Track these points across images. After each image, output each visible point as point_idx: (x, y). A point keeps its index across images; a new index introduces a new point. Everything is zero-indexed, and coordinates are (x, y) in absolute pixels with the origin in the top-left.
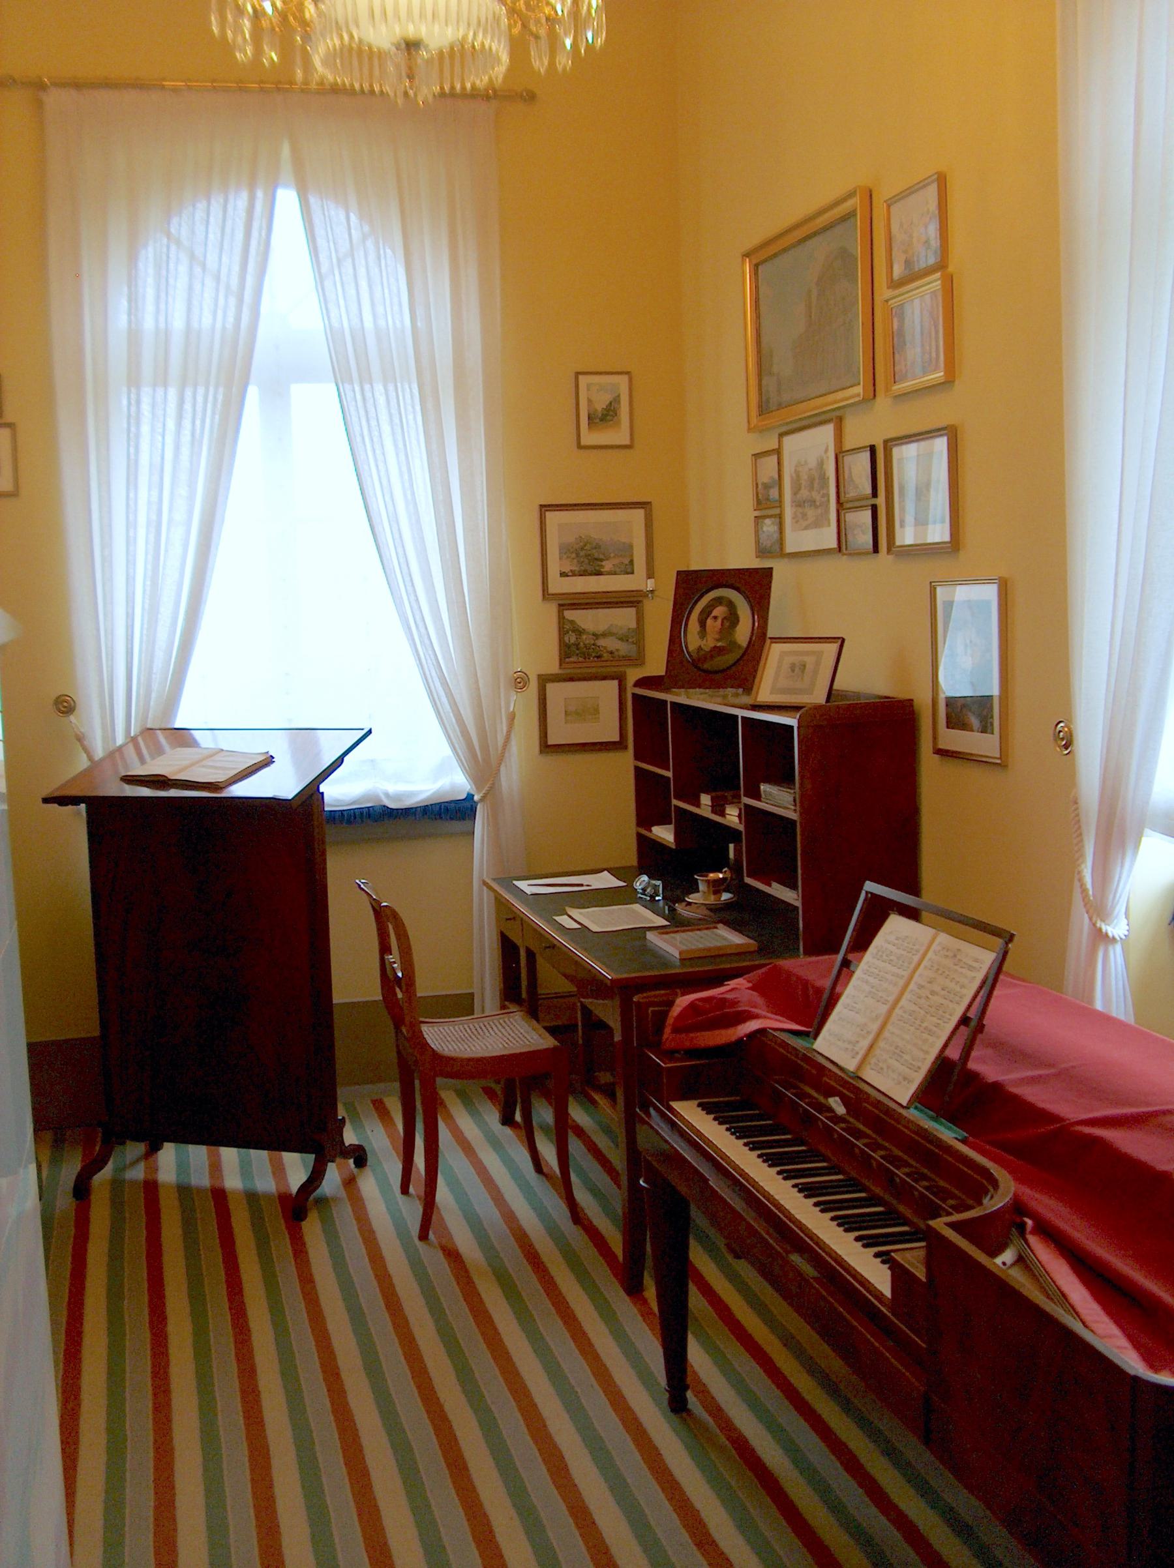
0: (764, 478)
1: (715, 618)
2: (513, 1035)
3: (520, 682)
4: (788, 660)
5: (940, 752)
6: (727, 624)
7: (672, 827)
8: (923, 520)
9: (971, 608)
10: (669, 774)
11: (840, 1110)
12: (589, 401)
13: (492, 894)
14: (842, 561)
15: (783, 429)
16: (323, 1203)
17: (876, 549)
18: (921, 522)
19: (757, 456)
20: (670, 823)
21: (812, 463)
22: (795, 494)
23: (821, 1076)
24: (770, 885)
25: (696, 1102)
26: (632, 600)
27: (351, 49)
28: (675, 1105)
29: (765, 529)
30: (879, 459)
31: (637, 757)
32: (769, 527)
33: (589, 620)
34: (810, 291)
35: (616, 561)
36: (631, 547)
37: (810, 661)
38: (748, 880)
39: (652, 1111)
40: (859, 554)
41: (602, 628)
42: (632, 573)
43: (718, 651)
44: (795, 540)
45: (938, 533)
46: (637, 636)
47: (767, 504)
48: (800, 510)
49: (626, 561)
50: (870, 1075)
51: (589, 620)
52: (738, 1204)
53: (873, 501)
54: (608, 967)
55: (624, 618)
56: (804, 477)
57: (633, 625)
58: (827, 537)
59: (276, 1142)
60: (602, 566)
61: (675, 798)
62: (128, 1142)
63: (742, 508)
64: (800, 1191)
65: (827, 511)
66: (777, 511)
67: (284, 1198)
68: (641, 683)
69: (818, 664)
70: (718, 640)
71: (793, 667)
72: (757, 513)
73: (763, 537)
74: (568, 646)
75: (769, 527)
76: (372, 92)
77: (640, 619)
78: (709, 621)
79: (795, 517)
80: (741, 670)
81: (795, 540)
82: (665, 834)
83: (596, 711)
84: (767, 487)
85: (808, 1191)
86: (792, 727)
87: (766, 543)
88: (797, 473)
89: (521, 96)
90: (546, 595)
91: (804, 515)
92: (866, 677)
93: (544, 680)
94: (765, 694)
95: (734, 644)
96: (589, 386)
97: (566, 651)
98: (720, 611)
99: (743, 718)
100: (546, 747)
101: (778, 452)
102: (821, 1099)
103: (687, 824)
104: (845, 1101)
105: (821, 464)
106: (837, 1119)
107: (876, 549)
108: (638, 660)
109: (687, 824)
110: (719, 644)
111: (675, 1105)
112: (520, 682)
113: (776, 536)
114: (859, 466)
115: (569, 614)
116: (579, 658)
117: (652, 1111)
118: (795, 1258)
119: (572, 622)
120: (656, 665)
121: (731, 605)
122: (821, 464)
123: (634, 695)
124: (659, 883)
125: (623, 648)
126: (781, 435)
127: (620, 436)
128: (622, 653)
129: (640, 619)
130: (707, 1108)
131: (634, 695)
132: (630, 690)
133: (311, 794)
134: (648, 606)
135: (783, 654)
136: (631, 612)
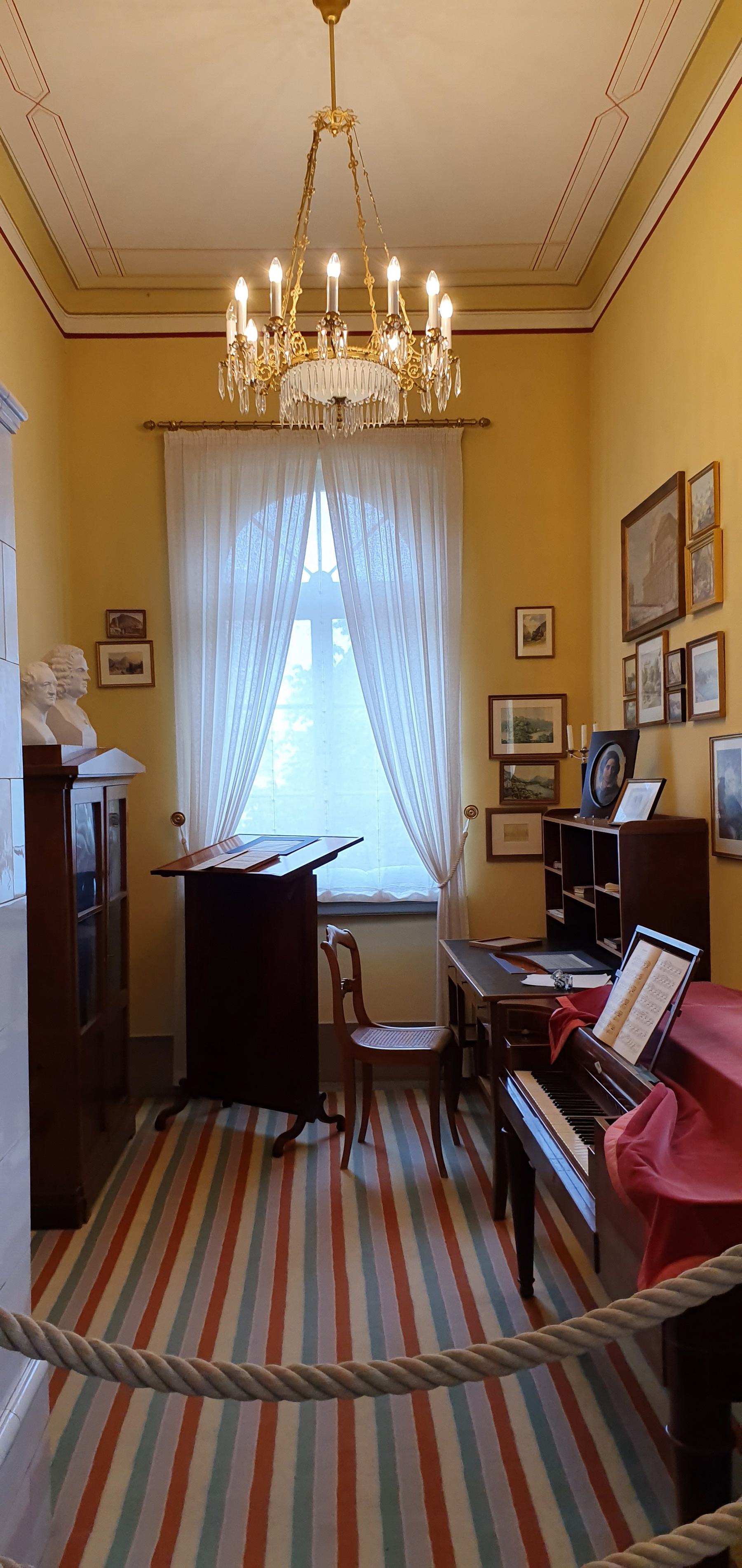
0: (629, 675)
3: (471, 812)
5: (715, 853)
7: (562, 911)
12: (524, 626)
19: (626, 659)
21: (653, 663)
22: (644, 683)
24: (603, 941)
27: (378, 401)
30: (685, 654)
34: (652, 545)
35: (541, 734)
36: (551, 724)
41: (530, 778)
42: (552, 742)
46: (555, 784)
53: (683, 687)
54: (484, 989)
55: (546, 772)
56: (649, 671)
57: (552, 777)
62: (317, 1121)
63: (617, 695)
66: (634, 697)
72: (625, 698)
73: (628, 715)
74: (507, 789)
76: (303, 427)
77: (557, 773)
82: (558, 914)
83: (526, 834)
84: (631, 680)
88: (646, 669)
89: (480, 423)
90: (492, 756)
93: (490, 812)
95: (615, 786)
96: (524, 616)
97: (504, 793)
99: (595, 832)
100: (491, 857)
101: (635, 656)
103: (572, 907)
105: (657, 663)
108: (556, 800)
112: (471, 812)
114: (675, 661)
116: (512, 798)
122: (657, 663)
125: (545, 793)
126: (638, 644)
127: (545, 649)
128: (544, 795)
129: (557, 773)
133: (304, 878)
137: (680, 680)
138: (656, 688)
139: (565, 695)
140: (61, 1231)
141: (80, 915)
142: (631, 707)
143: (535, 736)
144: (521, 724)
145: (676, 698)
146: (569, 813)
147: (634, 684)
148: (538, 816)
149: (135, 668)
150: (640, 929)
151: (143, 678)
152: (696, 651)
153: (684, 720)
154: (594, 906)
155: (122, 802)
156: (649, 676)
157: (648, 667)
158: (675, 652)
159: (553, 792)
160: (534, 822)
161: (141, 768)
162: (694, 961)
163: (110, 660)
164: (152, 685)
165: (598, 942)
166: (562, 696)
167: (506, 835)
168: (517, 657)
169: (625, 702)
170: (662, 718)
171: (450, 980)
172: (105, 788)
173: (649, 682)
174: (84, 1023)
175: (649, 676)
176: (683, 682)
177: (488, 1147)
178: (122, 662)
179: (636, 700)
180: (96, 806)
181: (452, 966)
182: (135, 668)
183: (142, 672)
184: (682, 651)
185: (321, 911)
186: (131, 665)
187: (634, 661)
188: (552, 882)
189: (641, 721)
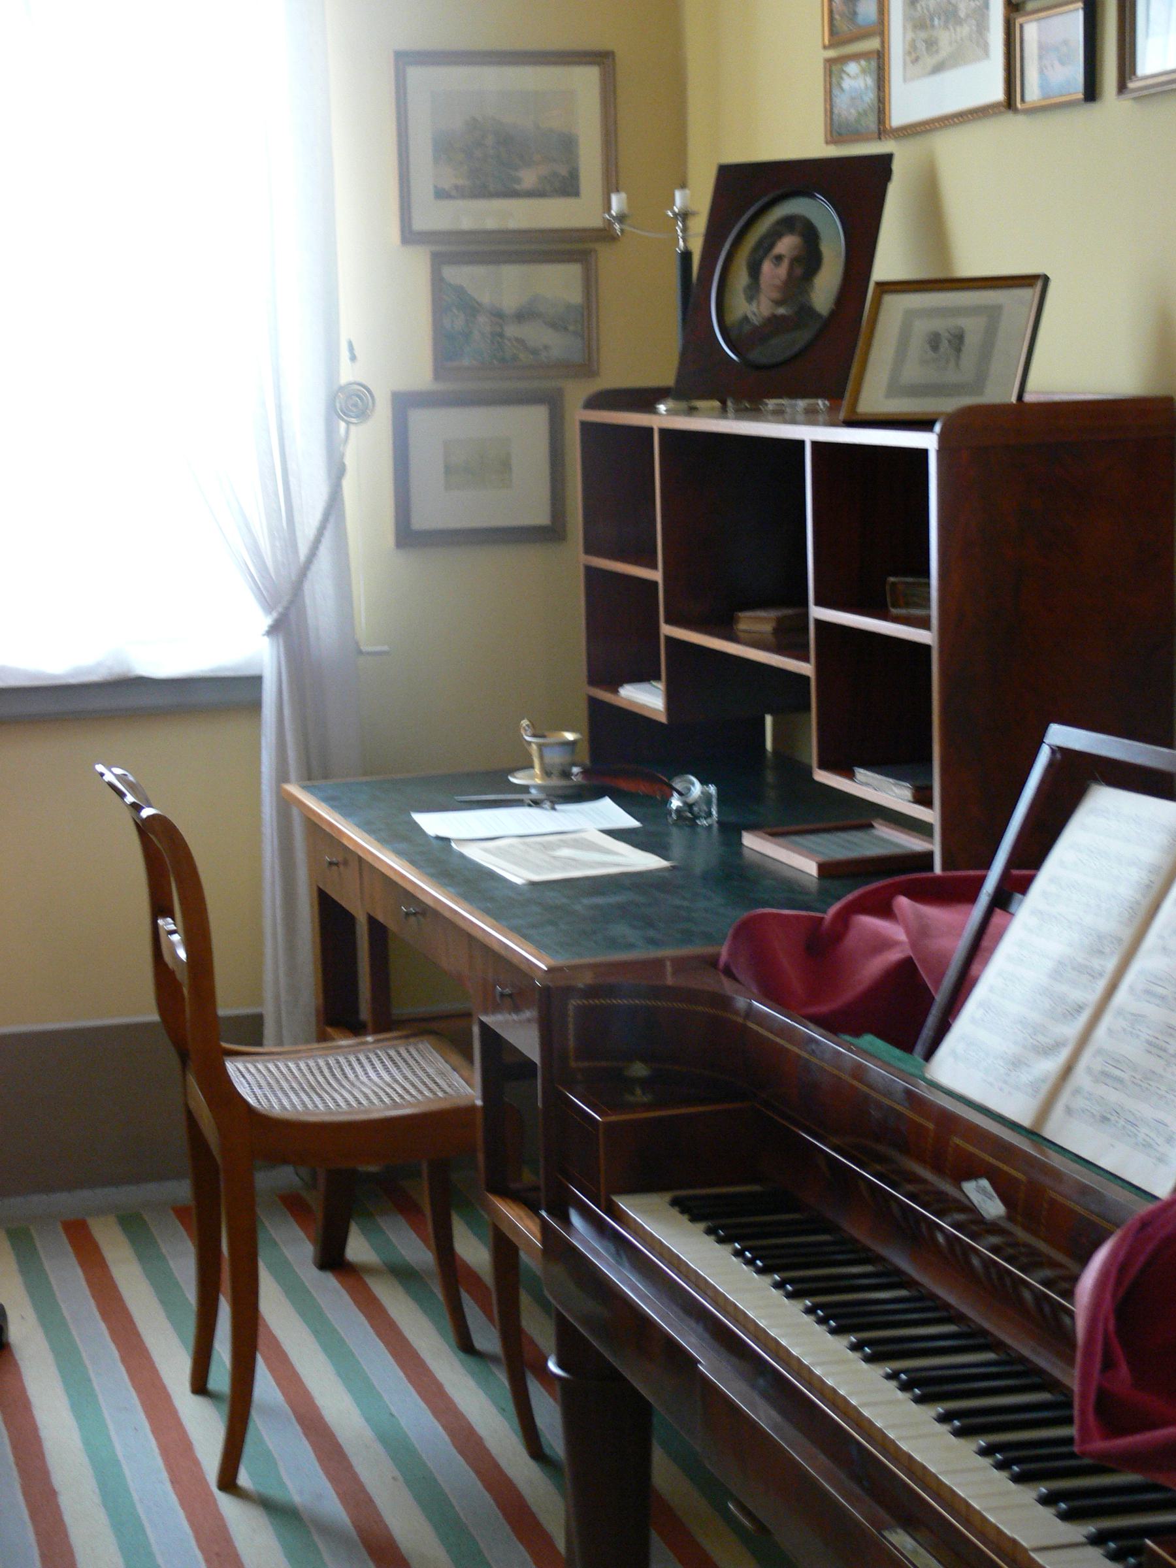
1: (779, 258)
4: (922, 328)
6: (799, 271)
7: (660, 686)
10: (656, 575)
11: (992, 1207)
17: (1091, 92)
20: (657, 678)
23: (952, 1141)
24: (850, 776)
25: (668, 1196)
28: (624, 1203)
29: (847, 83)
31: (589, 550)
32: (856, 80)
37: (973, 327)
38: (823, 777)
39: (576, 1219)
43: (775, 325)
44: (911, 101)
46: (584, 319)
48: (923, 35)
52: (763, 1415)
54: (540, 946)
57: (575, 296)
58: (983, 82)
60: (519, 181)
61: (669, 621)
64: (905, 1387)
65: (982, 27)
66: (873, 44)
68: (596, 402)
69: (991, 332)
70: (778, 303)
71: (934, 341)
72: (831, 53)
73: (842, 103)
75: (856, 80)
77: (590, 283)
78: (767, 267)
79: (913, 55)
80: (821, 354)
81: (911, 101)
82: (647, 698)
83: (505, 465)
85: (923, 1387)
90: (410, 236)
91: (931, 44)
95: (806, 312)
98: (787, 245)
99: (816, 445)
100: (408, 536)
102: (947, 1187)
103: (689, 673)
104: (1004, 1189)
106: (977, 1224)
107: (1091, 92)
109: (689, 673)
110: (781, 311)
111: (624, 1203)
113: (870, 97)
117: (576, 1219)
118: (901, 1540)
119: (460, 291)
121: (810, 235)
123: (586, 427)
130: (691, 1210)
131: (586, 427)
132: (578, 415)
135: (911, 315)
136: (572, 272)
144: (490, 140)
146: (645, 399)
154: (807, 669)
165: (823, 777)
166: (601, 58)
167: (449, 470)
169: (830, 62)
177: (555, 1399)
189: (898, 117)
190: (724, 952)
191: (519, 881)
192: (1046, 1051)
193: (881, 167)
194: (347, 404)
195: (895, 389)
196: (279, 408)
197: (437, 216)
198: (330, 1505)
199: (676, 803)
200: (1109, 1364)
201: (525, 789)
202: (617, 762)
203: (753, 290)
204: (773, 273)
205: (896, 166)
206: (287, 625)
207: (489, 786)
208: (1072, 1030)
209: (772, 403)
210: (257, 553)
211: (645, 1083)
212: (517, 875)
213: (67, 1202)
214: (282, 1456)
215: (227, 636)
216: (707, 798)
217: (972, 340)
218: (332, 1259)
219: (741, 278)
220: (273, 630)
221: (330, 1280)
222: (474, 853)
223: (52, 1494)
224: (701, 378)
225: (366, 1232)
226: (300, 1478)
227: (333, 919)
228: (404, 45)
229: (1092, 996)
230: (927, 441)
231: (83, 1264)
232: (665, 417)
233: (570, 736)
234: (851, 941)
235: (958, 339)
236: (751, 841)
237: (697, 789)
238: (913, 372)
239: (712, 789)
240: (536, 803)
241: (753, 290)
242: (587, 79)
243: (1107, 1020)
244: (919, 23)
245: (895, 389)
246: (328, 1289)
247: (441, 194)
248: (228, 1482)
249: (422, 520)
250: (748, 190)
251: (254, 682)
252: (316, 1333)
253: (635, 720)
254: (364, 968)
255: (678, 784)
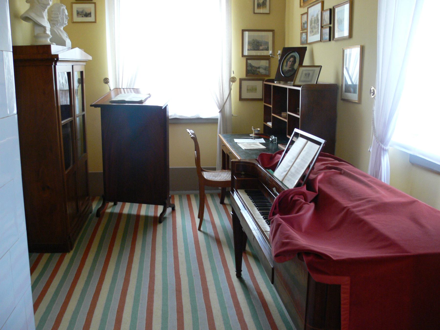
0: (304, 22)
2: (225, 176)
4: (304, 72)
8: (342, 30)
9: (353, 54)
10: (271, 106)
13: (316, 164)
14: (321, 44)
15: (308, 6)
16: (165, 218)
17: (330, 40)
18: (342, 30)
19: (302, 15)
21: (315, 16)
22: (311, 25)
26: (267, 58)
30: (332, 12)
32: (304, 36)
33: (254, 63)
37: (311, 73)
40: (325, 41)
43: (289, 71)
45: (346, 33)
47: (304, 29)
49: (267, 47)
50: (286, 183)
51: (254, 63)
53: (330, 25)
54: (240, 156)
55: (264, 63)
56: (313, 20)
57: (268, 65)
58: (317, 37)
59: (156, 203)
65: (318, 29)
66: (306, 31)
67: (155, 218)
73: (302, 39)
74: (249, 71)
78: (289, 62)
79: (310, 32)
80: (290, 76)
82: (270, 124)
83: (256, 90)
84: (304, 24)
86: (299, 90)
87: (303, 40)
88: (312, 19)
90: (243, 56)
91: (313, 31)
92: (326, 78)
94: (297, 83)
95: (293, 69)
99: (289, 89)
100: (241, 99)
101: (307, 13)
103: (275, 121)
105: (317, 15)
108: (268, 76)
109: (275, 121)
114: (327, 15)
115: (249, 61)
116: (251, 73)
119: (250, 64)
120: (273, 76)
122: (317, 15)
124: (276, 138)
134: (272, 60)
137: (329, 23)
138: (316, 26)
139: (274, 30)
140: (61, 254)
141: (63, 122)
142: (304, 36)
143: (261, 48)
144: (256, 42)
145: (327, 31)
147: (306, 25)
148: (261, 82)
149: (88, 15)
150: (296, 130)
151: (92, 19)
152: (337, 10)
153: (330, 40)
155: (82, 73)
156: (313, 22)
157: (313, 18)
158: (327, 10)
159: (268, 72)
160: (259, 85)
161: (90, 58)
162: (322, 145)
163: (77, 11)
164: (95, 22)
166: (272, 31)
167: (247, 90)
168: (254, 13)
169: (301, 33)
170: (320, 39)
171: (223, 150)
172: (73, 66)
173: (313, 25)
174: (66, 168)
175: (313, 22)
176: (330, 23)
178: (82, 12)
179: (307, 33)
180: (69, 74)
181: (224, 145)
182: (88, 15)
183: (91, 16)
184: (330, 10)
185: (170, 122)
186: (86, 13)
187: (306, 16)
188: (267, 110)
189: (309, 42)
190: (258, 159)
191: (243, 149)
192: (285, 171)
193: (305, 49)
194: (232, 80)
195: (300, 81)
196: (222, 80)
197: (246, 53)
198: (213, 234)
199: (271, 139)
200: (275, 209)
201: (252, 136)
202: (265, 134)
203: (286, 66)
204: (289, 63)
205: (307, 49)
206: (222, 111)
207: (245, 135)
208: (288, 169)
209: (289, 82)
210: (218, 101)
211: (244, 175)
212: (244, 148)
213: (188, 192)
214: (208, 227)
215: (215, 113)
216: (275, 139)
217: (311, 75)
218: (222, 202)
219: (285, 64)
220: (220, 112)
221: (221, 205)
222: (240, 145)
223: (176, 228)
224: (279, 78)
225: (228, 199)
226: (209, 229)
227: (223, 153)
228: (243, 29)
229: (291, 164)
230: (300, 89)
231: (188, 200)
232: (276, 84)
233: (259, 129)
234: (276, 158)
235: (309, 74)
236: (279, 145)
237: (274, 137)
238: (303, 79)
239: (276, 138)
240: (252, 138)
241: (286, 66)
242: (270, 34)
243: (292, 168)
244: (311, 28)
245: (300, 81)
246: (221, 207)
247: (248, 50)
248: (199, 229)
249: (243, 97)
250: (287, 51)
251: (218, 119)
252: (227, 215)
253: (268, 127)
254: (226, 161)
255: (271, 137)
